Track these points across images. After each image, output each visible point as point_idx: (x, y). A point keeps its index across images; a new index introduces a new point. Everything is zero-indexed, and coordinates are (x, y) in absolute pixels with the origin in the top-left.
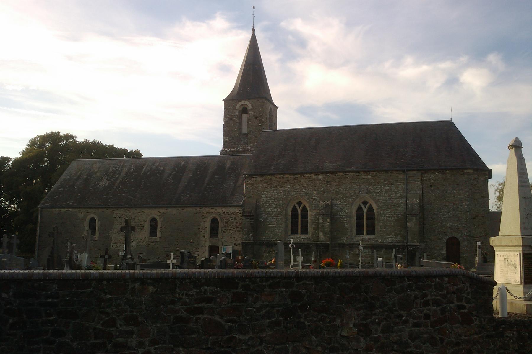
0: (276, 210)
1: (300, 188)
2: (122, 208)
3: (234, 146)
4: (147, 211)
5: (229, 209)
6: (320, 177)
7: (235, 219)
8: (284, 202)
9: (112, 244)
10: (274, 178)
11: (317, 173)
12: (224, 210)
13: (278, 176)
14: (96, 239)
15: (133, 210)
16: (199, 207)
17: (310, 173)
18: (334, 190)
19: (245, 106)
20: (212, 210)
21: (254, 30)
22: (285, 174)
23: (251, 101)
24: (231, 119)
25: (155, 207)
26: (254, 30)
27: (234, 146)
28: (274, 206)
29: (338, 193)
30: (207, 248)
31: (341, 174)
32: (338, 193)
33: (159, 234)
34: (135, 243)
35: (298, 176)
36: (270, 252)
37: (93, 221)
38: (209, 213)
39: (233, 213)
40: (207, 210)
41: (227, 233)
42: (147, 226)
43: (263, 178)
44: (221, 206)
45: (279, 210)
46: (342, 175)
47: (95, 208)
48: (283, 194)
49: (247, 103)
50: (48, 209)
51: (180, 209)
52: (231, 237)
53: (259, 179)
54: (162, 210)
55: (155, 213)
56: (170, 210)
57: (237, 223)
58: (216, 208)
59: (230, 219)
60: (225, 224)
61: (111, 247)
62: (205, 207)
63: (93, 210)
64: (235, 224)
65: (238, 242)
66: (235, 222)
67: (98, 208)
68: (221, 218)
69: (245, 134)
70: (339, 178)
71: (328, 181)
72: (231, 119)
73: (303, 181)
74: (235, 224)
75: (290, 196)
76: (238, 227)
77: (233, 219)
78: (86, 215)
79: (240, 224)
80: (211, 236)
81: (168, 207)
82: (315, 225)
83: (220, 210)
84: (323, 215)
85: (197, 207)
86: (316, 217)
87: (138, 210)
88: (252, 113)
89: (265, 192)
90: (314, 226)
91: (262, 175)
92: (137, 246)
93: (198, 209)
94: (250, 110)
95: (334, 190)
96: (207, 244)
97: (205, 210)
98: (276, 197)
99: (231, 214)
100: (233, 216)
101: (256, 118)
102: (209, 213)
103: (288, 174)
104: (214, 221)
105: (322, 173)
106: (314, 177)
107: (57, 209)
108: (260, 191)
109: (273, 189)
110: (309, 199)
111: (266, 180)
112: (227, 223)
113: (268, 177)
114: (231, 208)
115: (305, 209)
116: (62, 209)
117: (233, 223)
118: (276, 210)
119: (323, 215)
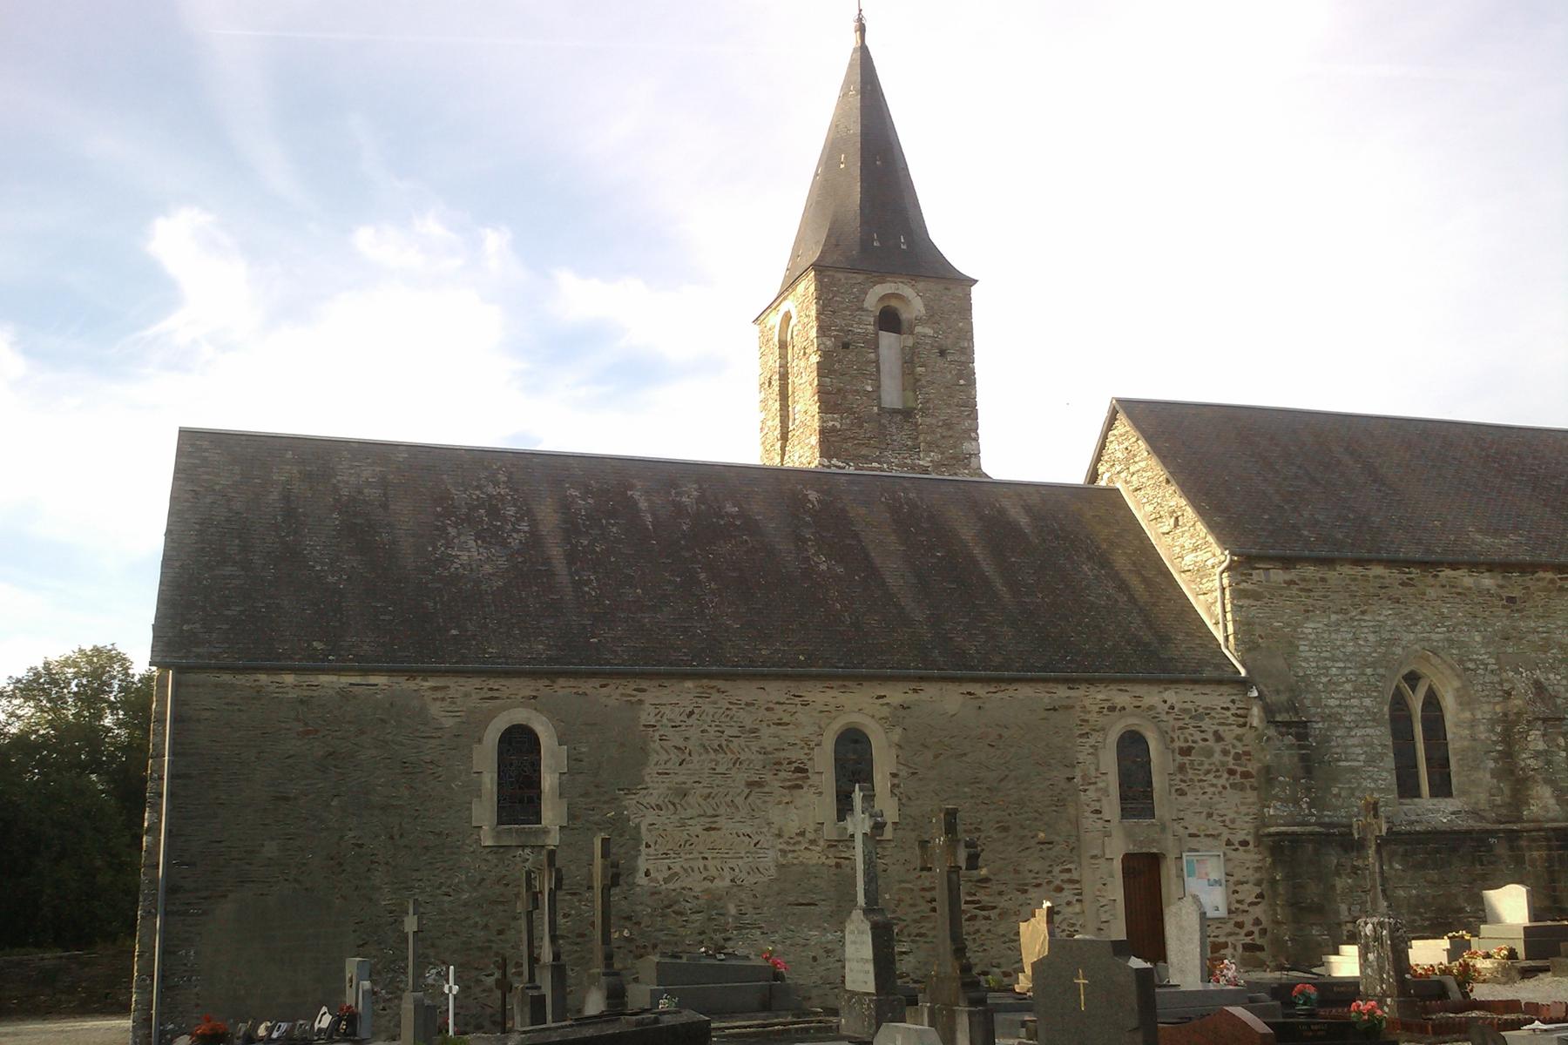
0: (1355, 702)
1: (1426, 619)
2: (686, 676)
3: (864, 451)
4: (819, 696)
5: (1189, 696)
6: (1488, 581)
7: (1218, 738)
8: (1381, 671)
9: (642, 865)
10: (1332, 575)
11: (1474, 566)
12: (1171, 696)
13: (1347, 570)
14: (553, 840)
15: (745, 691)
16: (1066, 681)
17: (1454, 566)
18: (1535, 631)
19: (894, 303)
20: (1122, 699)
21: (862, 29)
22: (1370, 561)
23: (921, 285)
24: (846, 346)
25: (861, 679)
26: (862, 29)
27: (864, 451)
28: (1348, 687)
29: (1545, 647)
30: (1117, 865)
31: (1549, 575)
32: (1545, 647)
33: (552, 814)
34: (771, 854)
35: (1415, 572)
36: (1355, 869)
37: (519, 747)
38: (1112, 709)
39: (1208, 712)
40: (1100, 694)
41: (1190, 798)
42: (824, 763)
43: (1292, 575)
44: (1159, 682)
45: (1367, 702)
46: (1552, 581)
47: (534, 675)
48: (1372, 638)
49: (907, 291)
50: (226, 678)
51: (979, 690)
52: (1210, 815)
53: (1278, 576)
54: (896, 694)
55: (861, 706)
56: (931, 691)
57: (1225, 753)
58: (1139, 690)
59: (1198, 736)
60: (1178, 757)
61: (641, 879)
62: (1091, 682)
63: (525, 687)
64: (1217, 757)
65: (1241, 836)
66: (1218, 748)
67: (553, 676)
68: (1163, 733)
69: (895, 412)
70: (1545, 589)
71: (1511, 600)
72: (846, 346)
73: (1432, 593)
74: (1217, 757)
75: (1399, 651)
76: (1231, 772)
77: (1210, 736)
78: (467, 713)
79: (1237, 757)
80: (1126, 813)
81: (921, 679)
82: (1496, 760)
83: (1153, 697)
84: (1545, 720)
85: (1056, 680)
86: (1492, 731)
87: (775, 691)
88: (930, 332)
89: (1309, 627)
90: (1491, 764)
91: (1287, 562)
92: (780, 867)
93: (1062, 692)
94: (919, 320)
95: (1535, 631)
96: (1117, 848)
97: (1095, 697)
98: (1349, 649)
99: (1199, 717)
100: (1206, 724)
101: (942, 353)
102: (1112, 709)
103: (1380, 562)
104: (1132, 744)
105: (1491, 567)
106: (1467, 579)
107: (289, 679)
108: (1288, 625)
109: (1334, 617)
110: (1461, 662)
111: (1304, 580)
112: (1185, 752)
113: (1310, 571)
114: (1198, 688)
115: (1432, 702)
116: (324, 679)
117: (1209, 753)
118: (1355, 702)
119: (1545, 720)
